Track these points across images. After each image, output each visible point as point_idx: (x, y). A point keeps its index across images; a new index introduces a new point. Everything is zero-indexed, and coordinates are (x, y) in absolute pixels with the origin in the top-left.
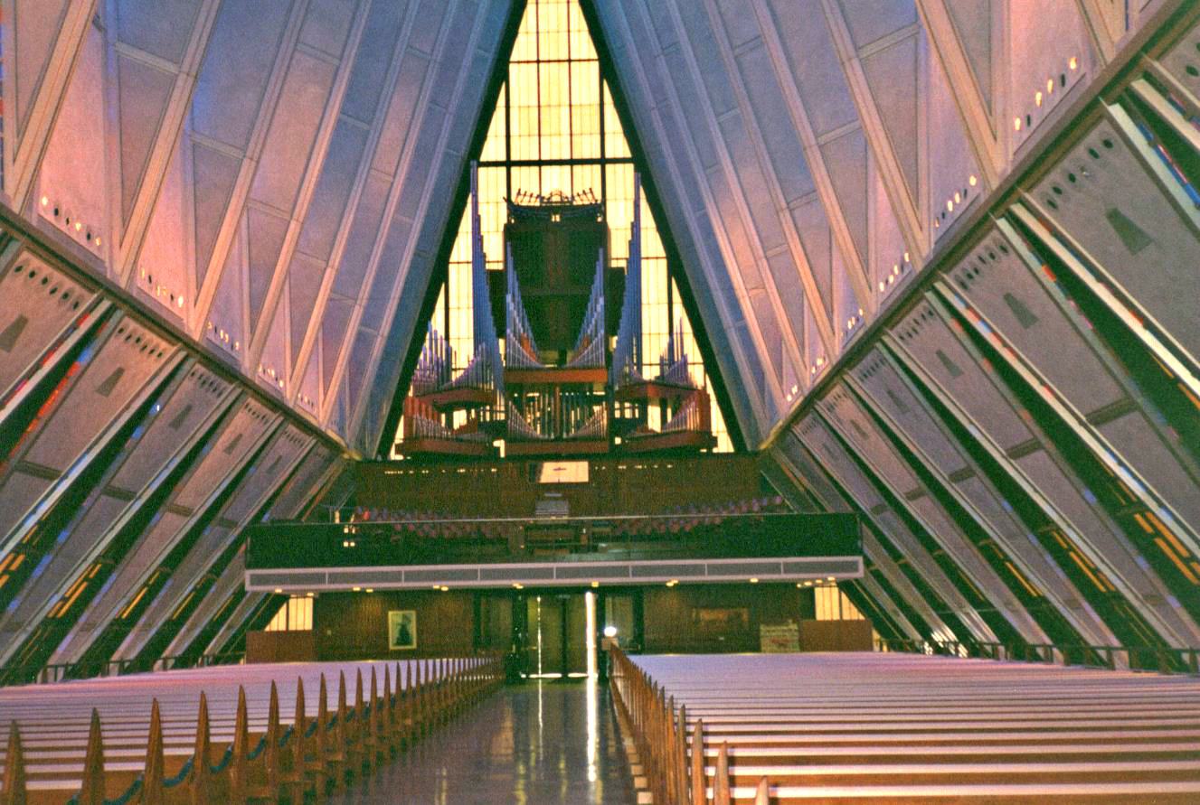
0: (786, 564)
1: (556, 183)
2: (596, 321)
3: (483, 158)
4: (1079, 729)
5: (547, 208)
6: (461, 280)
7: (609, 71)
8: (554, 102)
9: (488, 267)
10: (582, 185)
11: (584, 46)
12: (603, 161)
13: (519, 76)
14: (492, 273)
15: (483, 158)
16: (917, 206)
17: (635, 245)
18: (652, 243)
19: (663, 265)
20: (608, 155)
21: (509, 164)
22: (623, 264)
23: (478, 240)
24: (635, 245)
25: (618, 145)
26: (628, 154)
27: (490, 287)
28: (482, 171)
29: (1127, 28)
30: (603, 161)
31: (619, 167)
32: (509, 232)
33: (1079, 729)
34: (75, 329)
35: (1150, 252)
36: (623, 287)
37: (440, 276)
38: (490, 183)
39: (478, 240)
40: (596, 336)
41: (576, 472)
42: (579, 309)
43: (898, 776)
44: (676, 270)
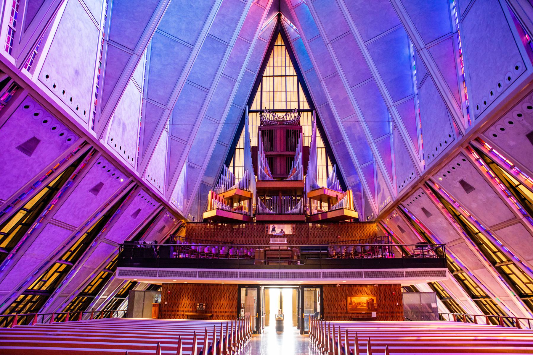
0: (407, 272)
2: (299, 163)
6: (240, 155)
7: (301, 80)
11: (291, 71)
13: (267, 82)
14: (253, 147)
16: (393, 182)
17: (313, 137)
18: (320, 143)
25: (305, 105)
29: (425, 169)
31: (305, 113)
34: (132, 235)
37: (231, 154)
40: (299, 167)
41: (288, 229)
42: (290, 159)
43: (31, 346)
44: (329, 152)
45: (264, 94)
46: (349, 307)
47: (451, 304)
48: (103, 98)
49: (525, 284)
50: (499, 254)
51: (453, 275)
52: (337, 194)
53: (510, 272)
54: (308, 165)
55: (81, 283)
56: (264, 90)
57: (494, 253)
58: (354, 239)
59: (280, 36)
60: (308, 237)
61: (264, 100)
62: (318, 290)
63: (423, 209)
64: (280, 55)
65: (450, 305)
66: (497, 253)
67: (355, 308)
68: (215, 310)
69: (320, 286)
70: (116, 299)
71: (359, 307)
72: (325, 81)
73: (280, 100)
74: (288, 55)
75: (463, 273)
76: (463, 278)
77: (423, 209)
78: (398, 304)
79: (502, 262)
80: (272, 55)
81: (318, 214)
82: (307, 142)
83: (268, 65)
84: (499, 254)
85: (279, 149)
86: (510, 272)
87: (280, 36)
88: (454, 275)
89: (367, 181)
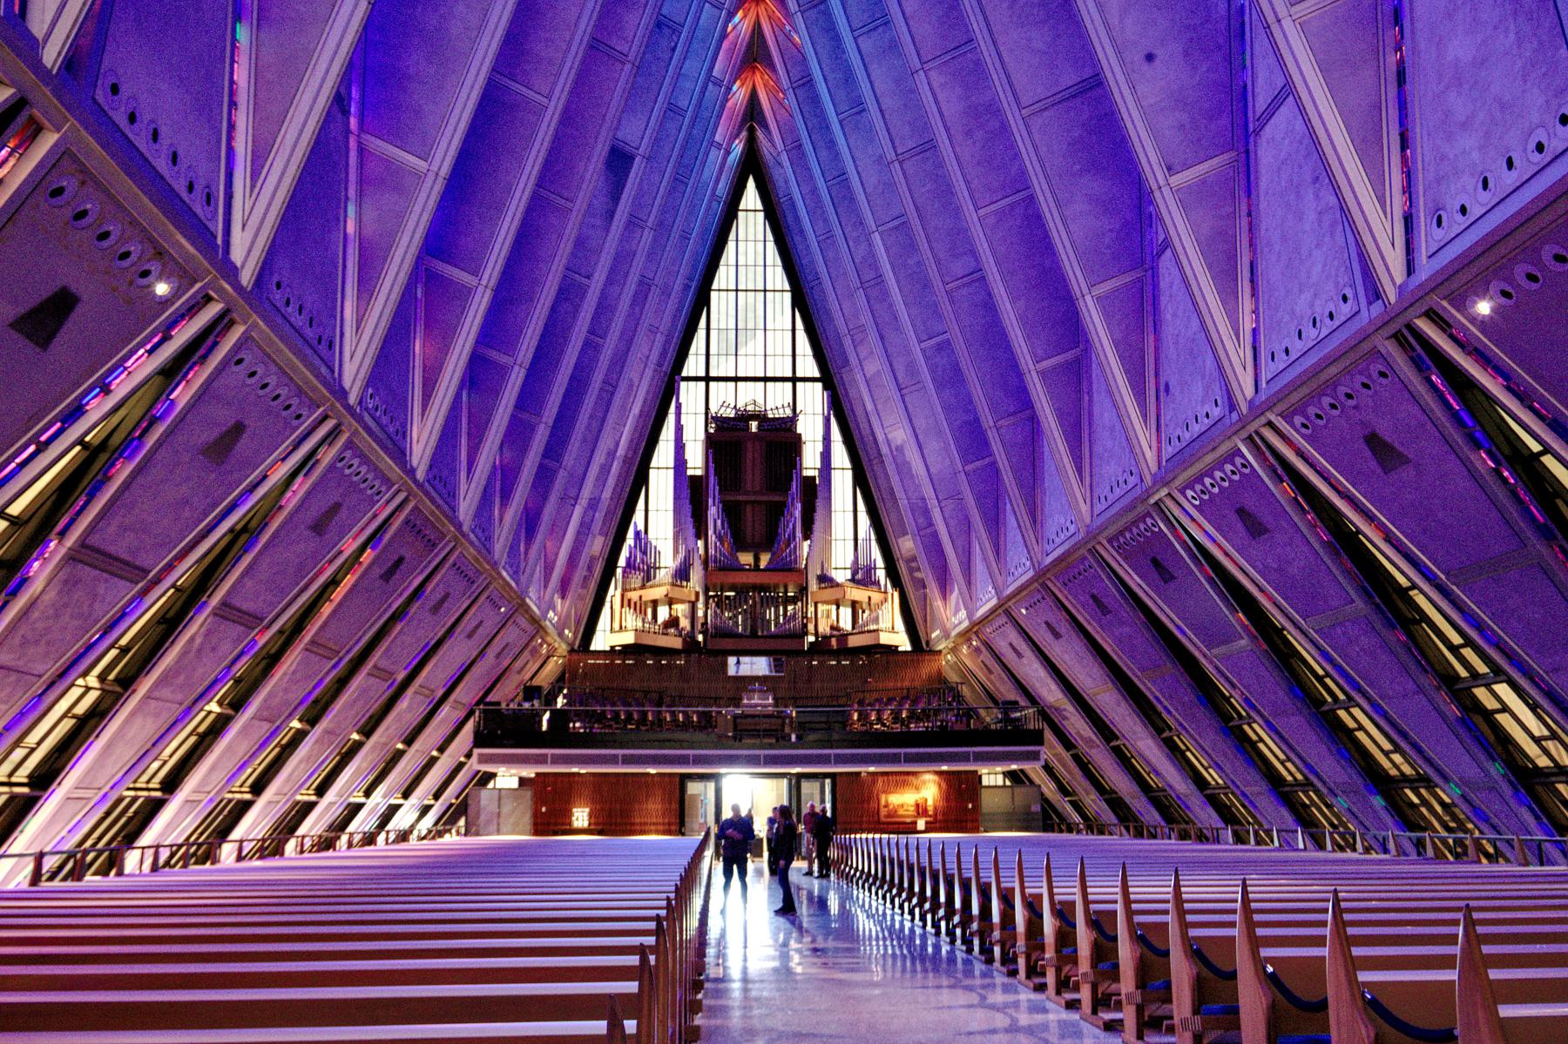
1: (749, 396)
3: (684, 374)
4: (283, 913)
5: (743, 418)
6: (661, 483)
7: (802, 301)
8: (692, 410)
9: (690, 472)
10: (776, 400)
11: (778, 277)
12: (794, 380)
14: (693, 478)
15: (684, 374)
17: (826, 456)
18: (840, 456)
19: (849, 474)
20: (799, 374)
21: (707, 379)
22: (815, 473)
23: (680, 447)
24: (826, 456)
25: (808, 367)
26: (817, 375)
27: (691, 493)
28: (683, 385)
30: (794, 380)
32: (711, 442)
33: (283, 913)
35: (1407, 474)
36: (814, 493)
37: (641, 479)
38: (690, 396)
39: (680, 447)
44: (861, 480)
45: (713, 334)
46: (883, 812)
47: (1416, 800)
49: (1537, 741)
50: (1467, 652)
51: (1112, 748)
52: (870, 593)
53: (1355, 726)
54: (814, 511)
55: (297, 767)
56: (713, 325)
57: (1454, 649)
58: (899, 685)
59: (751, 184)
60: (809, 681)
61: (713, 350)
62: (828, 781)
63: (1011, 644)
64: (751, 237)
65: (1412, 805)
66: (1462, 650)
67: (893, 813)
68: (638, 820)
69: (832, 776)
70: (135, 799)
71: (901, 812)
72: (881, 234)
73: (751, 359)
74: (770, 236)
75: (1352, 710)
76: (1351, 724)
77: (1011, 644)
78: (970, 806)
79: (1475, 675)
80: (732, 236)
81: (831, 636)
82: (810, 462)
83: (723, 261)
84: (1467, 652)
85: (753, 476)
86: (1495, 705)
87: (751, 184)
88: (1112, 748)
89: (1061, 415)
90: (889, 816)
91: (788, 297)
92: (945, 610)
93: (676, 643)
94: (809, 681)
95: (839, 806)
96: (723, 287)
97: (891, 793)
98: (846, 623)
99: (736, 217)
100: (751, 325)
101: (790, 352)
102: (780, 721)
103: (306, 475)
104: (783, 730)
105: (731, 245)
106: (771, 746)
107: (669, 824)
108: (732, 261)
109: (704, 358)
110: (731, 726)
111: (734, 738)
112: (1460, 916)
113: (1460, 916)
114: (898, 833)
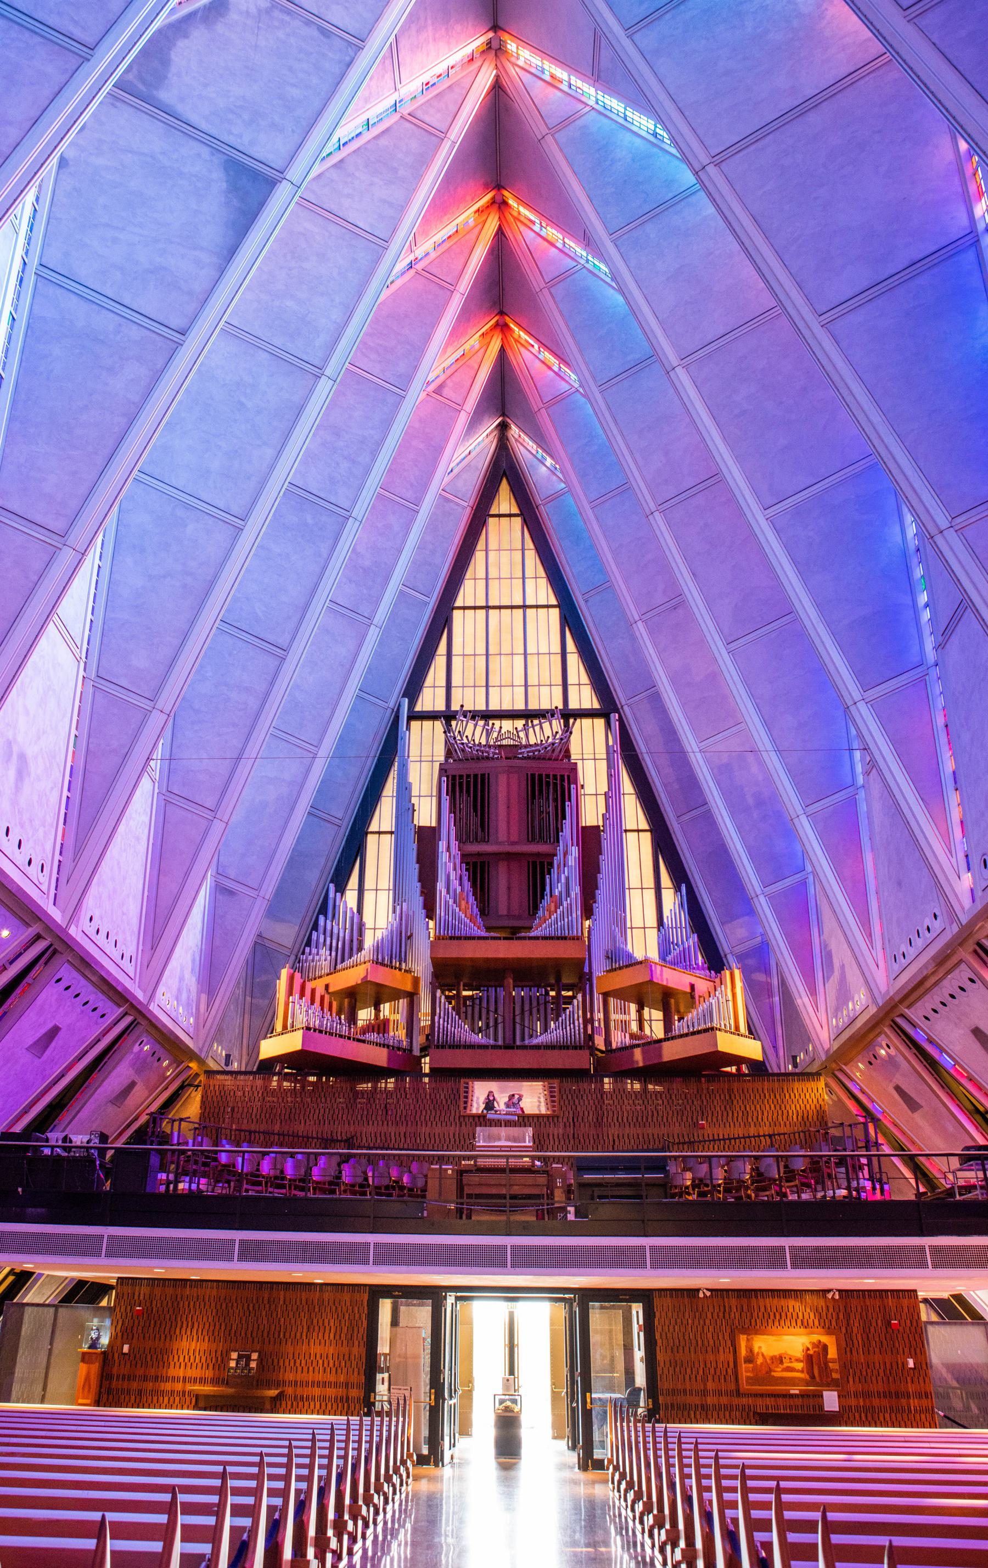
25: (583, 697)
45: (456, 661)
46: (745, 1371)
48: (343, 75)
52: (693, 980)
54: (600, 852)
56: (456, 649)
58: (752, 1131)
61: (456, 680)
62: (637, 1309)
64: (505, 545)
67: (765, 1373)
68: (290, 1376)
71: (778, 1373)
74: (529, 544)
78: (911, 1363)
80: (481, 545)
90: (753, 1380)
91: (555, 613)
92: (816, 1008)
93: (379, 1057)
94: (599, 1123)
95: (660, 1356)
96: (470, 603)
97: (757, 1332)
98: (656, 1030)
99: (484, 523)
100: (506, 649)
101: (559, 680)
102: (542, 1179)
103: (46, 964)
104: (551, 1196)
105: (479, 556)
106: (526, 1230)
107: (346, 1385)
108: (481, 573)
109: (443, 691)
110: (452, 1186)
111: (460, 1212)
112: (772, 1497)
113: (772, 1497)
114: (776, 1414)
